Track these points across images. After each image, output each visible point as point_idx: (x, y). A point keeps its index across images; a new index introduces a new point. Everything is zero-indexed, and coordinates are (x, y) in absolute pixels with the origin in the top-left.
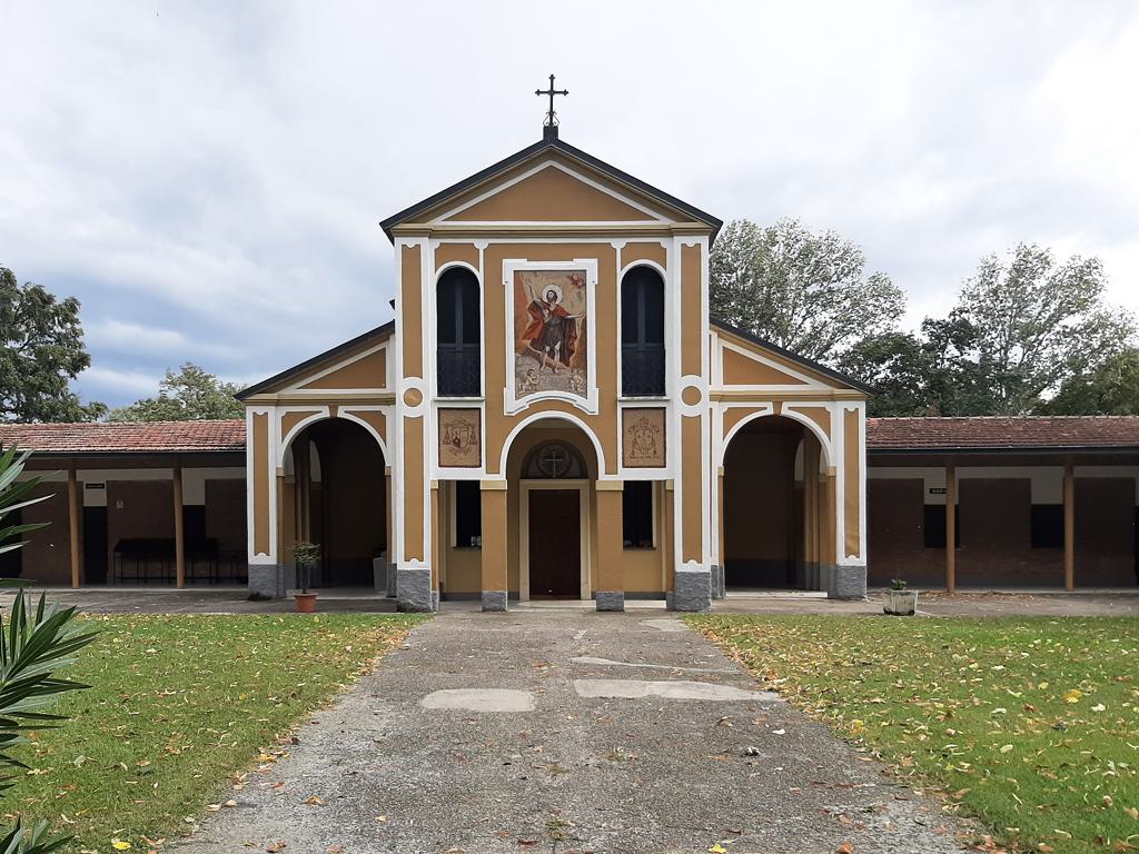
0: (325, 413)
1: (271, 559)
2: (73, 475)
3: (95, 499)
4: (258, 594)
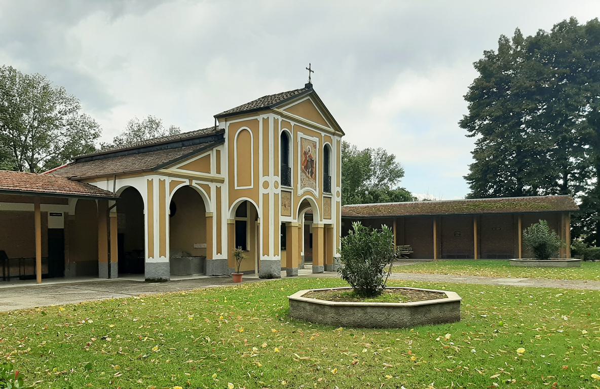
0: (187, 183)
1: (224, 256)
2: (37, 207)
3: (56, 223)
4: (161, 278)
